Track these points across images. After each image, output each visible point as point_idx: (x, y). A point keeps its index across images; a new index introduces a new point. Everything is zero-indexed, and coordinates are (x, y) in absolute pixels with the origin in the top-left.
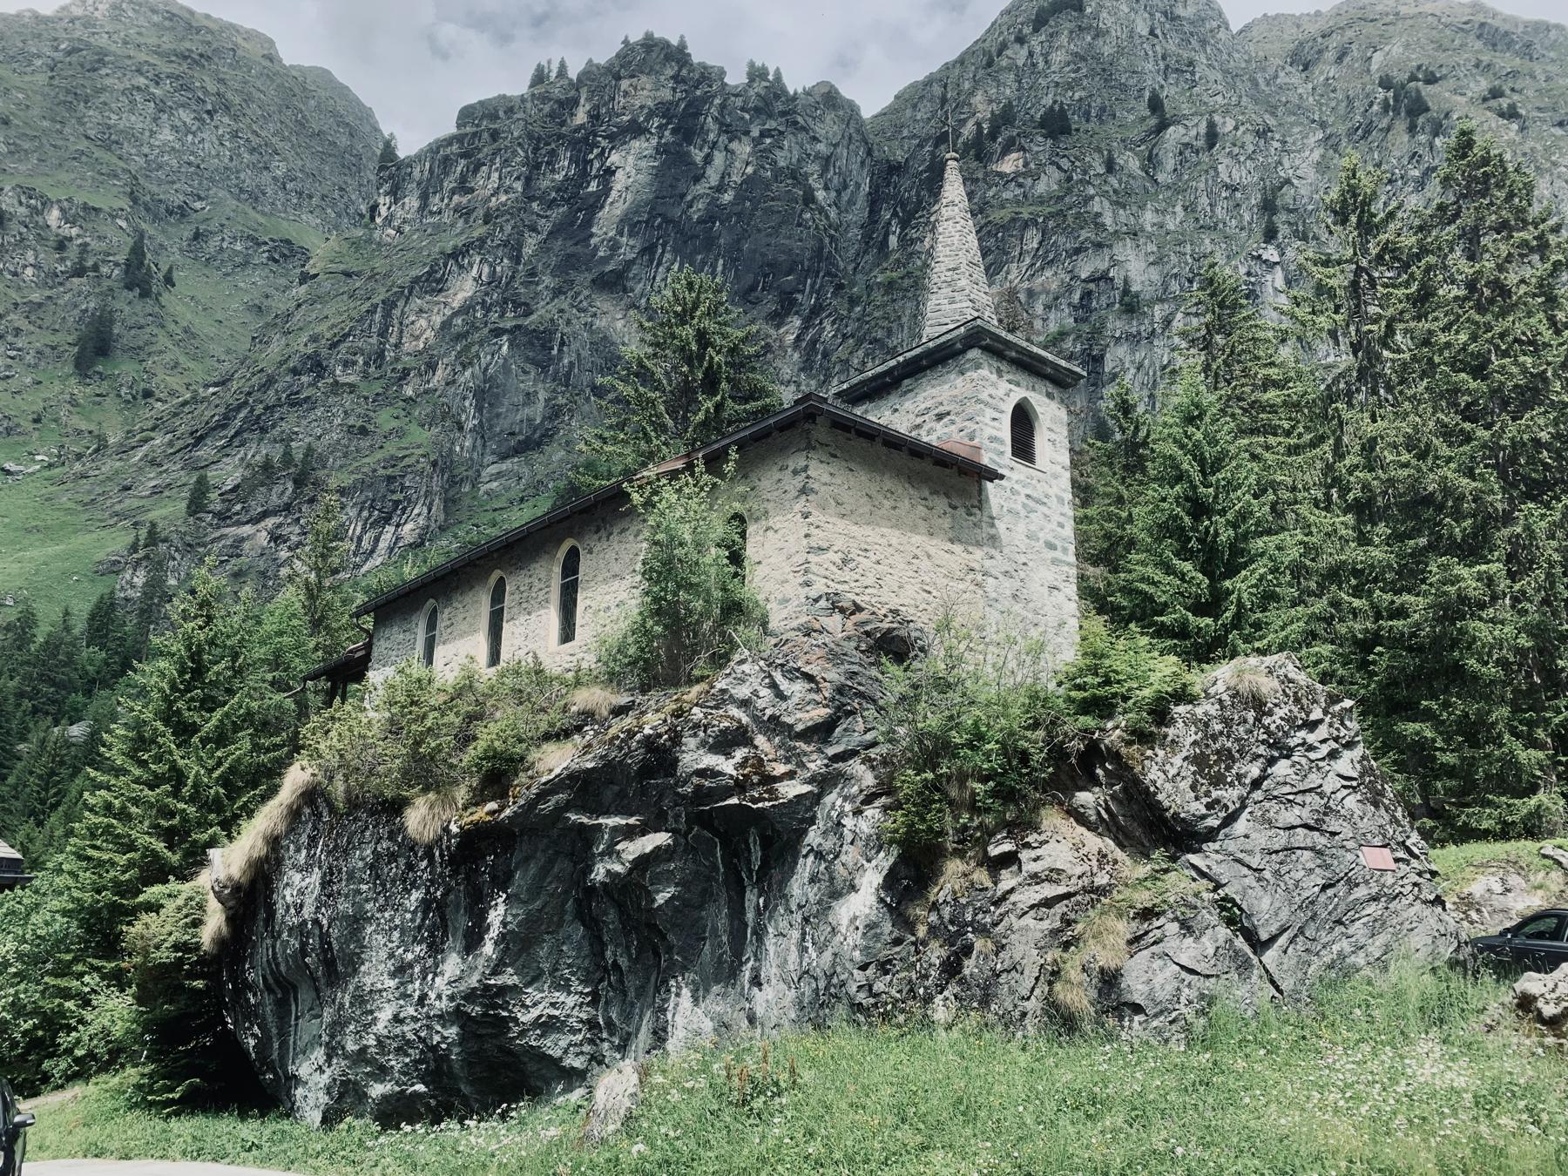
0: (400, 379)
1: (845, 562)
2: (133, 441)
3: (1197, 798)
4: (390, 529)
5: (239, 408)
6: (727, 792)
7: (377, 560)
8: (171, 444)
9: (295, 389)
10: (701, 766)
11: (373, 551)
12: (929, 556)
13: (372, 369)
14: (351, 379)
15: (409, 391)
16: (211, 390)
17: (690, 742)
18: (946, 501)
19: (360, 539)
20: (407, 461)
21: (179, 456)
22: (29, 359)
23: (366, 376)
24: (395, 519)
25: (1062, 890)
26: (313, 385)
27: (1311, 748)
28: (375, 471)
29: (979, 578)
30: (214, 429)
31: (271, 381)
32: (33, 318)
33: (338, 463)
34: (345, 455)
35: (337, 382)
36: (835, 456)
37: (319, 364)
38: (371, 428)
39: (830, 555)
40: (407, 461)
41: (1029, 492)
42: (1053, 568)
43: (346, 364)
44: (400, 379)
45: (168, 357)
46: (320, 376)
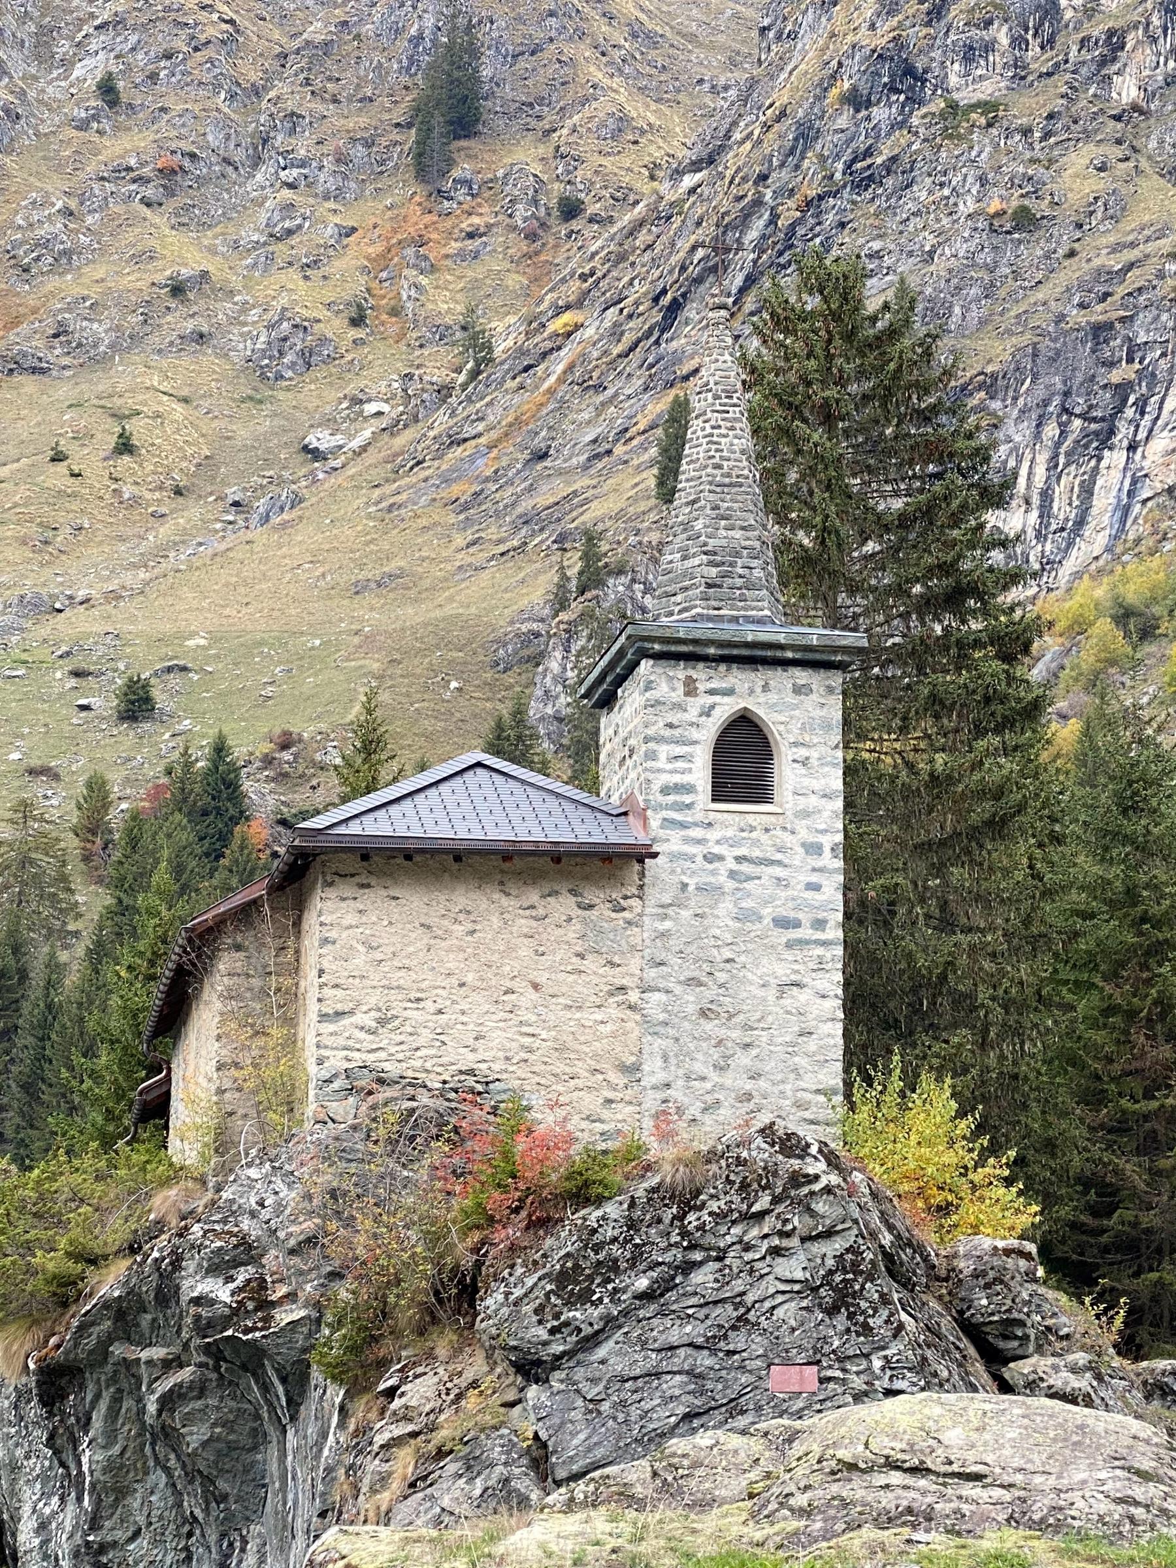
0: (1103, 62)
1: (382, 1022)
2: (540, 341)
3: (540, 1322)
4: (1115, 458)
5: (746, 218)
6: (226, 1322)
7: (1094, 541)
8: (616, 333)
9: (861, 143)
10: (195, 1294)
11: (1081, 522)
12: (536, 986)
13: (1035, 49)
14: (987, 90)
15: (1126, 90)
16: (689, 181)
17: (190, 1265)
18: (571, 900)
19: (1046, 495)
20: (1135, 278)
21: (636, 356)
22: (326, 180)
23: (1019, 73)
24: (1124, 432)
25: (410, 1428)
26: (901, 124)
27: (748, 1248)
28: (1061, 318)
29: (634, 996)
30: (698, 281)
31: (806, 135)
32: (318, 83)
33: (974, 314)
34: (989, 292)
35: (953, 106)
36: (368, 886)
37: (909, 71)
38: (1041, 208)
39: (359, 1018)
40: (1135, 278)
41: (742, 851)
42: (789, 955)
43: (970, 54)
44: (1103, 62)
45: (601, 108)
46: (914, 100)
